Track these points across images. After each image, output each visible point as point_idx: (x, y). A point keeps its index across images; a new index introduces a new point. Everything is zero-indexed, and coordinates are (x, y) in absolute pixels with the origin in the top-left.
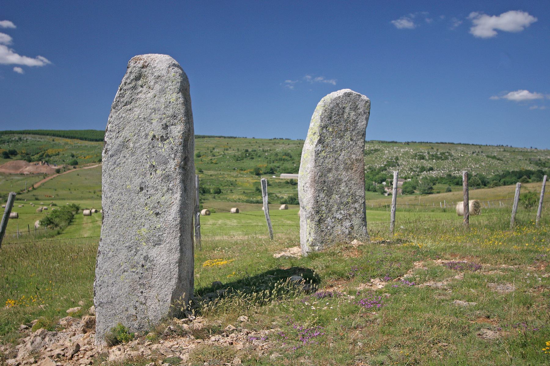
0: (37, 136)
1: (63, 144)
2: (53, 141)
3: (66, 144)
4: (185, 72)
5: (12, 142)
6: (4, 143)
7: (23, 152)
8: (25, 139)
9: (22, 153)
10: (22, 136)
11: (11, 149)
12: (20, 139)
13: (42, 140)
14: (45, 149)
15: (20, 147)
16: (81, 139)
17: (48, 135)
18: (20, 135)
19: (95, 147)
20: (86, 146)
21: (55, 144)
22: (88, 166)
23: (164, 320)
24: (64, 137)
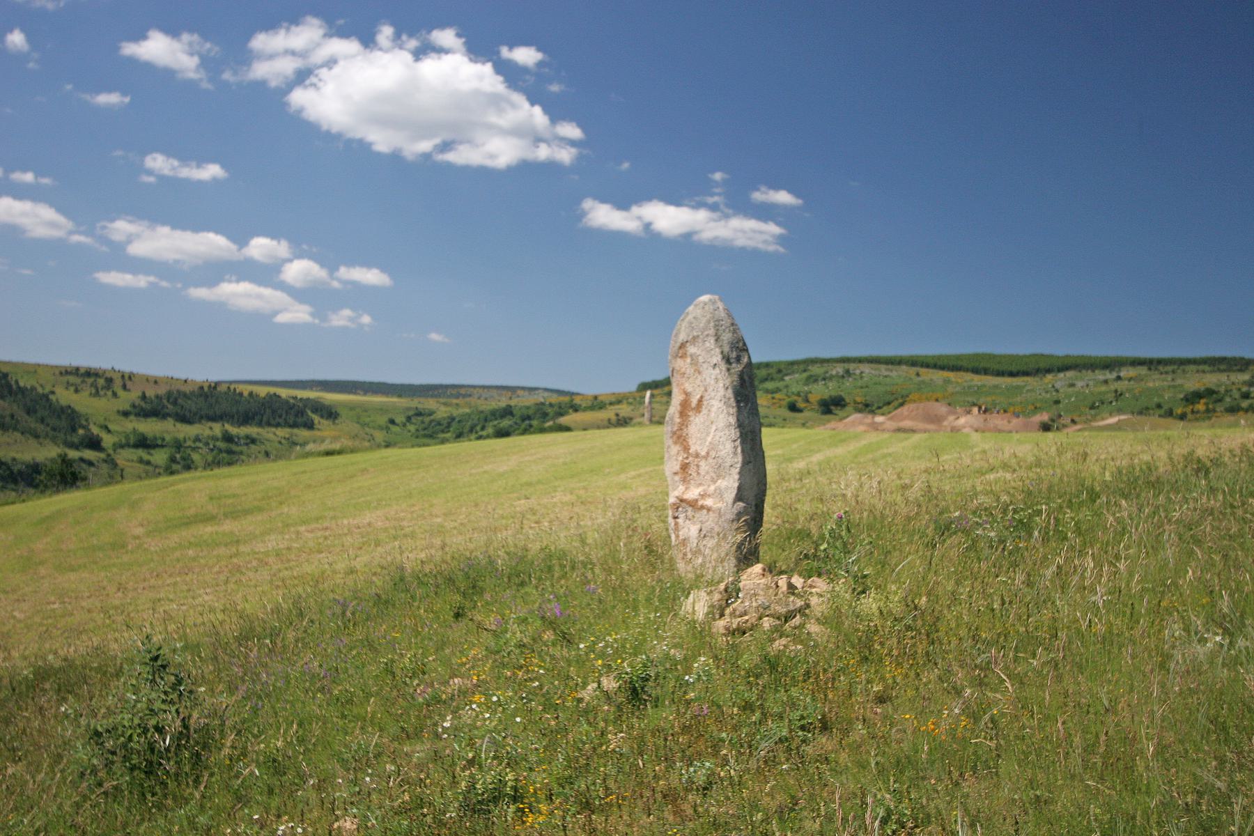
0: (883, 367)
1: (940, 382)
2: (918, 375)
3: (947, 381)
4: (737, 321)
5: (831, 378)
6: (816, 381)
7: (859, 399)
8: (858, 372)
9: (855, 402)
10: (852, 366)
11: (834, 393)
12: (847, 372)
13: (894, 374)
14: (904, 392)
15: (847, 389)
16: (976, 371)
17: (1049, 371)
18: (846, 366)
19: (1018, 387)
20: (996, 387)
21: (923, 382)
22: (259, 296)
23: (331, 63)
24: (942, 368)
